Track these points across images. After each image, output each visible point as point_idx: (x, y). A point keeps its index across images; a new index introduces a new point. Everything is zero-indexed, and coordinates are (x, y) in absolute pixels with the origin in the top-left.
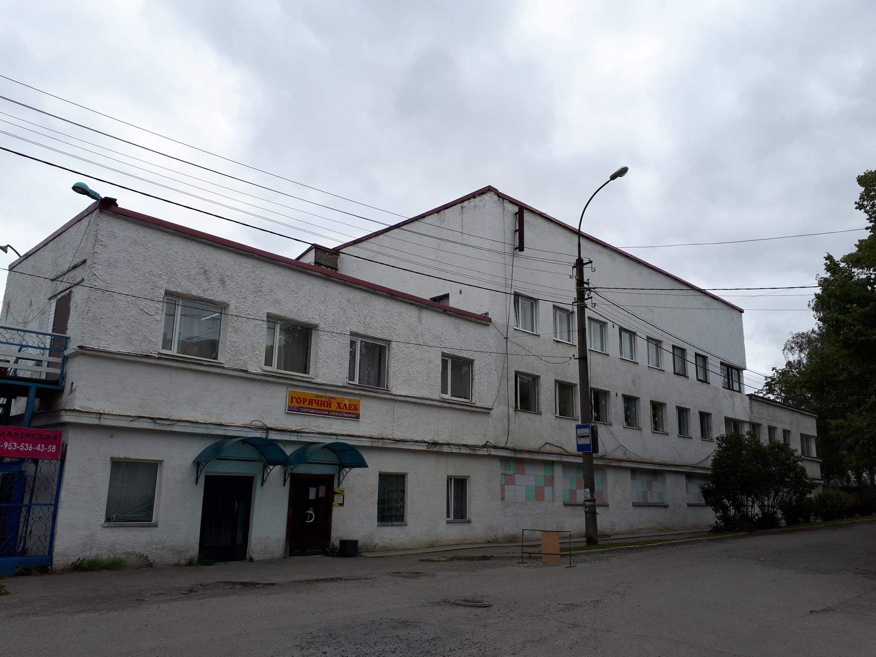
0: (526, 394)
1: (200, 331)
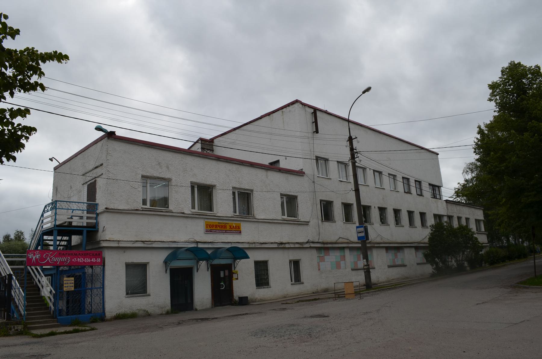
0: (327, 210)
1: (157, 192)
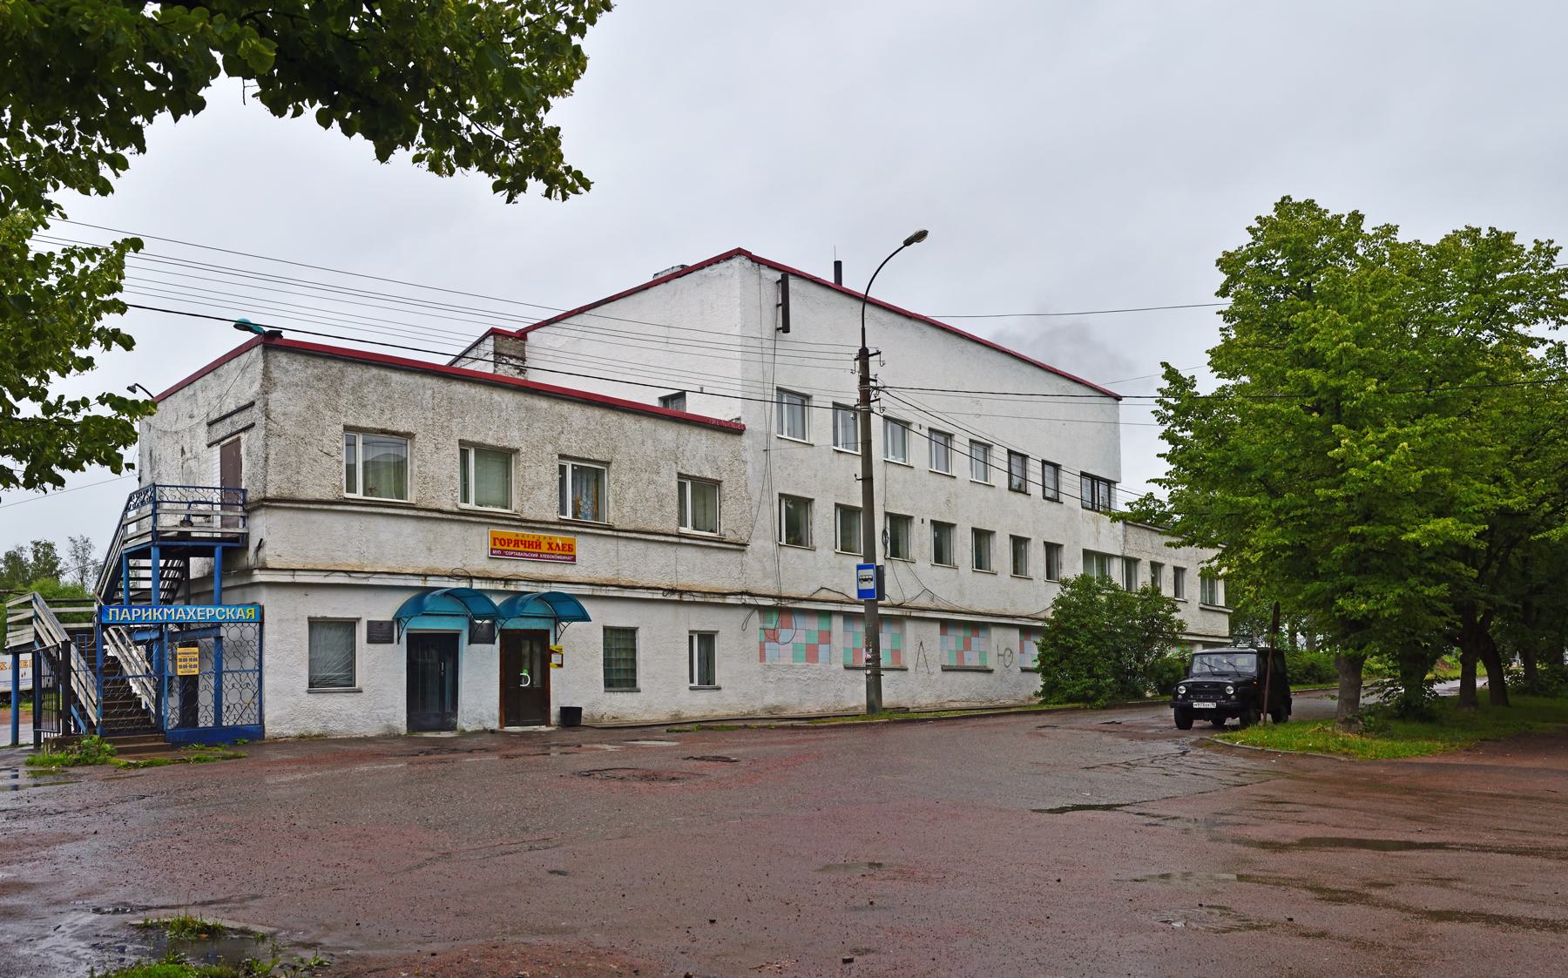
0: (795, 520)
